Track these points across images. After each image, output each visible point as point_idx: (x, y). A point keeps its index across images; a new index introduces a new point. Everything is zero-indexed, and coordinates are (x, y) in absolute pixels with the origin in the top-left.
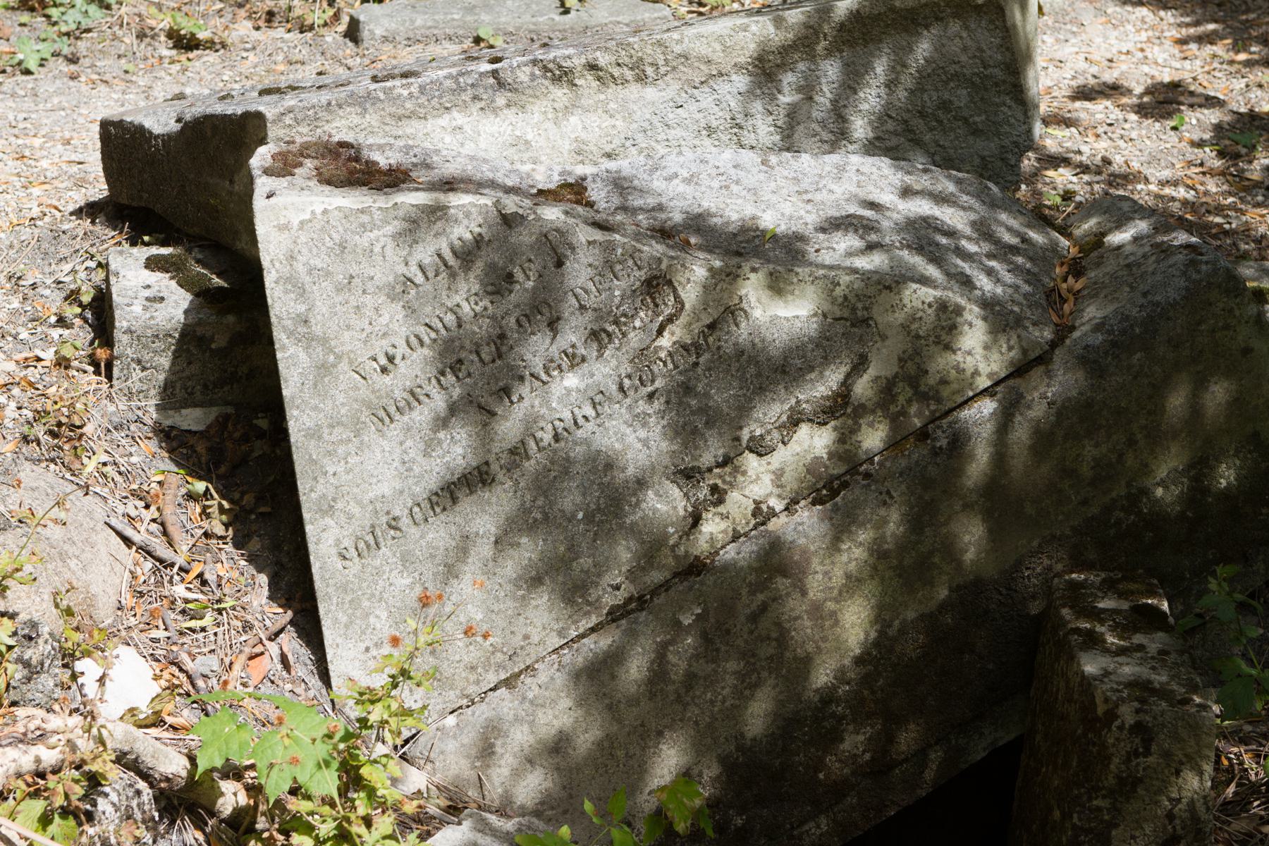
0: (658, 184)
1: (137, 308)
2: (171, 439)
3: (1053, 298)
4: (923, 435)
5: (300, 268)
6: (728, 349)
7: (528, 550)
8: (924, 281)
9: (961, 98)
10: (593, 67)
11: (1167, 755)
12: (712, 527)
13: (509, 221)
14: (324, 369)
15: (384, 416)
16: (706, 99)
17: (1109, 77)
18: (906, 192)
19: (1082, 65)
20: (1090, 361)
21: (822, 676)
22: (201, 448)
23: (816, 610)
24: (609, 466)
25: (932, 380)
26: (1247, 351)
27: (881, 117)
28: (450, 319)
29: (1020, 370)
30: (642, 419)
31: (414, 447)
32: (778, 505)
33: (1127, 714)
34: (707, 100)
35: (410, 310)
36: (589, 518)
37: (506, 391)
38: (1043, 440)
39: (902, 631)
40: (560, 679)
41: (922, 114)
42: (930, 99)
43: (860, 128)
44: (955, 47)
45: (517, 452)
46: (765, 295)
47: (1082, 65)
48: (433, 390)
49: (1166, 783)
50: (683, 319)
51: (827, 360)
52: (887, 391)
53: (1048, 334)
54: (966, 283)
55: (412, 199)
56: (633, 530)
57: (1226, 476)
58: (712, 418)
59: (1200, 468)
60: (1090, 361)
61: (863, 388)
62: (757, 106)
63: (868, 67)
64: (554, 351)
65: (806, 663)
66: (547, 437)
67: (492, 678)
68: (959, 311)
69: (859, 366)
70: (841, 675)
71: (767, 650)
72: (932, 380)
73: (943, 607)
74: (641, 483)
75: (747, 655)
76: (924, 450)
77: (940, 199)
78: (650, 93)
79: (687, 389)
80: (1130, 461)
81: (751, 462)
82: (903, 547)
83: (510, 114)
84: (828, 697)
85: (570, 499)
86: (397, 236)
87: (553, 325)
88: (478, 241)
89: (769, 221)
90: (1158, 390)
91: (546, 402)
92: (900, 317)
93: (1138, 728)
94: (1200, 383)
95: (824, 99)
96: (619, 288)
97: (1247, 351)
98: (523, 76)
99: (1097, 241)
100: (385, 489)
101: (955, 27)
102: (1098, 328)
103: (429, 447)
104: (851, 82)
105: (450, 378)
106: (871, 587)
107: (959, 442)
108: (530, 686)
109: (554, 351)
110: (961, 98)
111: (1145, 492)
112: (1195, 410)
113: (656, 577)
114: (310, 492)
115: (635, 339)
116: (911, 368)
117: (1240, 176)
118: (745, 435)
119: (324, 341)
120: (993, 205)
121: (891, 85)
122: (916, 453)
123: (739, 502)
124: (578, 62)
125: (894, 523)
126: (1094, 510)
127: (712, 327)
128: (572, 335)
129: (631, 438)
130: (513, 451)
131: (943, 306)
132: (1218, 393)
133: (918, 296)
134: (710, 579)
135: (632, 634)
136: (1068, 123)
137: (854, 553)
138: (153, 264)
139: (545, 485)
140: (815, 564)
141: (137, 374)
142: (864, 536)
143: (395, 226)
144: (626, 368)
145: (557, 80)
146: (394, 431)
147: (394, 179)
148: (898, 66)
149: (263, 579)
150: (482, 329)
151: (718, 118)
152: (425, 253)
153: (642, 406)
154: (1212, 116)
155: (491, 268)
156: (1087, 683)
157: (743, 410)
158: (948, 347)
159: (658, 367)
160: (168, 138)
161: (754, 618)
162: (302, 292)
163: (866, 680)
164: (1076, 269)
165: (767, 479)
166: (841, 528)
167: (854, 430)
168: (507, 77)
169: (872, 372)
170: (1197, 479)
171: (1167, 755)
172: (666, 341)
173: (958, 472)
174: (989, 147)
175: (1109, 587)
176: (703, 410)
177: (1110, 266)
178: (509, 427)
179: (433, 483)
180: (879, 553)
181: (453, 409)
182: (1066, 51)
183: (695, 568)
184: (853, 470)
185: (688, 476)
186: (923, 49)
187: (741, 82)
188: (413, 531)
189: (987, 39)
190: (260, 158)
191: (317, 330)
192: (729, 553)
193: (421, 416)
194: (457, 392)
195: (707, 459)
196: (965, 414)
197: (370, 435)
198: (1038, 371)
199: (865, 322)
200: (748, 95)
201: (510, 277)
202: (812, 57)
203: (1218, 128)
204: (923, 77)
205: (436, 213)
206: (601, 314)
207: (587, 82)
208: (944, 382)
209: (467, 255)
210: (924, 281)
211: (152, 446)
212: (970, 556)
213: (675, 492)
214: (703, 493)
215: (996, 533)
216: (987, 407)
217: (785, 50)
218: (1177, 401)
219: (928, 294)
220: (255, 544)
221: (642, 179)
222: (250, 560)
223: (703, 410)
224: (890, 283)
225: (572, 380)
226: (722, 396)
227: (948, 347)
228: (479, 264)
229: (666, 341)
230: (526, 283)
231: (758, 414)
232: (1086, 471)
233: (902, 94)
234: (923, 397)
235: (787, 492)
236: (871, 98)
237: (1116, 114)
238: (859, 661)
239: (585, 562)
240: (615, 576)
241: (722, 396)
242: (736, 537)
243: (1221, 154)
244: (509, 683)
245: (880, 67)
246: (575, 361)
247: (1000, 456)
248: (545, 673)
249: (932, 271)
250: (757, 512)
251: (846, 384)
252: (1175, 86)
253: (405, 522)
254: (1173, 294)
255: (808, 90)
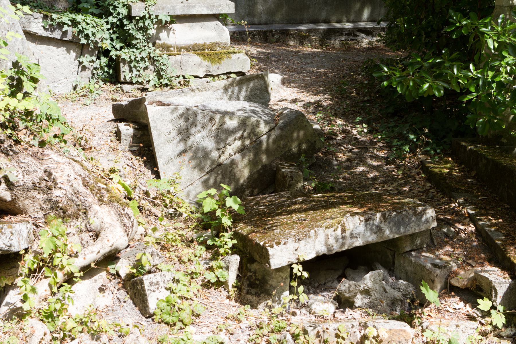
0: (210, 106)
1: (125, 131)
2: (132, 152)
3: (275, 120)
4: (255, 141)
5: (155, 118)
6: (224, 129)
7: (193, 163)
8: (254, 117)
9: (258, 93)
10: (198, 89)
11: (296, 180)
12: (223, 158)
13: (188, 110)
14: (159, 135)
15: (169, 142)
16: (216, 93)
17: (284, 98)
18: (250, 106)
19: (279, 97)
20: (281, 128)
21: (241, 181)
22: (137, 152)
23: (240, 171)
24: (206, 148)
25: (256, 133)
26: (306, 126)
27: (246, 96)
28: (179, 126)
29: (270, 130)
30: (210, 140)
31: (174, 146)
32: (233, 154)
33: (289, 175)
34: (217, 94)
35: (173, 124)
36: (203, 157)
37: (189, 137)
38: (274, 141)
39: (254, 173)
40: (200, 183)
41: (252, 96)
42: (253, 93)
43: (242, 98)
44: (257, 84)
45: (191, 147)
46: (229, 120)
47: (279, 97)
48: (177, 137)
49: (296, 185)
50: (216, 124)
51: (239, 130)
52: (249, 135)
53: (274, 125)
54: (261, 117)
55: (172, 107)
56: (210, 159)
57: (304, 147)
58: (222, 140)
59: (300, 145)
60: (281, 128)
61: (245, 134)
62: (225, 95)
63: (243, 88)
64: (196, 130)
65: (238, 180)
66: (195, 144)
67: (188, 184)
68: (260, 121)
69: (245, 131)
70: (244, 181)
71: (232, 177)
72: (256, 133)
73: (260, 169)
74: (211, 151)
75: (229, 178)
76: (256, 144)
77: (256, 107)
78: (207, 93)
79: (217, 135)
80: (289, 144)
81: (228, 147)
82: (253, 159)
83: (184, 97)
84: (243, 185)
85: (200, 154)
86: (171, 113)
87: (196, 126)
88: (183, 113)
89: (228, 110)
90: (292, 133)
91: (195, 138)
92: (251, 123)
93: (291, 177)
94: (299, 132)
95: (235, 93)
96: (206, 120)
97: (306, 126)
98: (186, 90)
99: (282, 113)
100: (170, 153)
101: (256, 81)
102: (282, 123)
103: (177, 146)
104: (240, 91)
105: (180, 135)
106: (249, 166)
107: (261, 142)
108: (195, 185)
109: (196, 130)
110: (258, 93)
111: (291, 149)
112: (298, 136)
113: (214, 166)
114: (158, 155)
115: (209, 128)
116: (253, 131)
117: (308, 111)
118: (227, 143)
119: (159, 130)
120: (264, 108)
121: (246, 91)
122: (254, 144)
123: (227, 154)
124: (195, 88)
125: (252, 156)
126: (283, 153)
127: (221, 125)
128: (199, 127)
129: (209, 144)
130: (190, 147)
131: (257, 121)
132: (302, 133)
133: (253, 119)
134: (223, 166)
135: (211, 175)
136: (277, 105)
137: (246, 161)
138: (125, 125)
139: (196, 152)
140: (239, 163)
141: (125, 142)
142: (247, 158)
143: (170, 111)
144: (208, 132)
145: (192, 91)
146: (171, 144)
147: (169, 105)
148: (247, 88)
149: (150, 171)
150: (184, 127)
151: (219, 97)
152: (175, 115)
153: (210, 138)
154: (303, 103)
155: (185, 117)
156: (283, 172)
157: (227, 139)
158: (258, 127)
159: (213, 132)
160: (126, 105)
161: (230, 172)
162: (155, 122)
163: (249, 182)
164: (278, 116)
165: (231, 150)
166: (243, 157)
167: (244, 141)
168: (184, 91)
169: (247, 132)
170: (299, 147)
171: (296, 180)
172: (214, 128)
173: (261, 147)
174: (263, 101)
175: (286, 163)
176: (220, 139)
177: (284, 115)
178: (189, 143)
179: (178, 152)
180: (249, 161)
181: (180, 140)
182: (277, 95)
183: (220, 165)
184: (245, 148)
185: (218, 149)
186: (251, 85)
187: (222, 91)
188: (175, 160)
189: (262, 83)
190: (146, 103)
191: (158, 128)
192: (226, 162)
193: (175, 141)
194: (181, 137)
195: (221, 147)
196: (262, 138)
197: (167, 145)
198: (273, 131)
199: (245, 124)
200: (223, 93)
201: (188, 119)
202: (233, 86)
203: (304, 104)
204: (252, 89)
205: (176, 109)
206: (203, 124)
207: (197, 91)
208: (258, 133)
209: (181, 115)
210: (254, 117)
211: (129, 152)
212: (264, 161)
213: (216, 152)
214: (221, 152)
215: (268, 157)
216: (265, 136)
217: (229, 85)
218: (295, 135)
219: (255, 119)
220: (148, 166)
221: (207, 105)
222: (147, 168)
223: (220, 139)
224: (249, 117)
225: (199, 135)
226: (223, 136)
227: (258, 127)
228: (183, 117)
229: (214, 128)
230: (191, 120)
231: (229, 139)
232: (281, 146)
233: (248, 92)
234: (255, 135)
235: (234, 152)
236: (243, 93)
237: (286, 103)
238: (247, 179)
239: (203, 164)
240: (208, 166)
241: (223, 136)
242: (226, 159)
243: (304, 108)
244: (191, 184)
245: (245, 88)
246: (199, 132)
247: (268, 144)
248: (197, 182)
249: (255, 116)
250: (230, 155)
251: (243, 134)
252: (296, 99)
253: (173, 159)
254: (293, 117)
255: (233, 92)
